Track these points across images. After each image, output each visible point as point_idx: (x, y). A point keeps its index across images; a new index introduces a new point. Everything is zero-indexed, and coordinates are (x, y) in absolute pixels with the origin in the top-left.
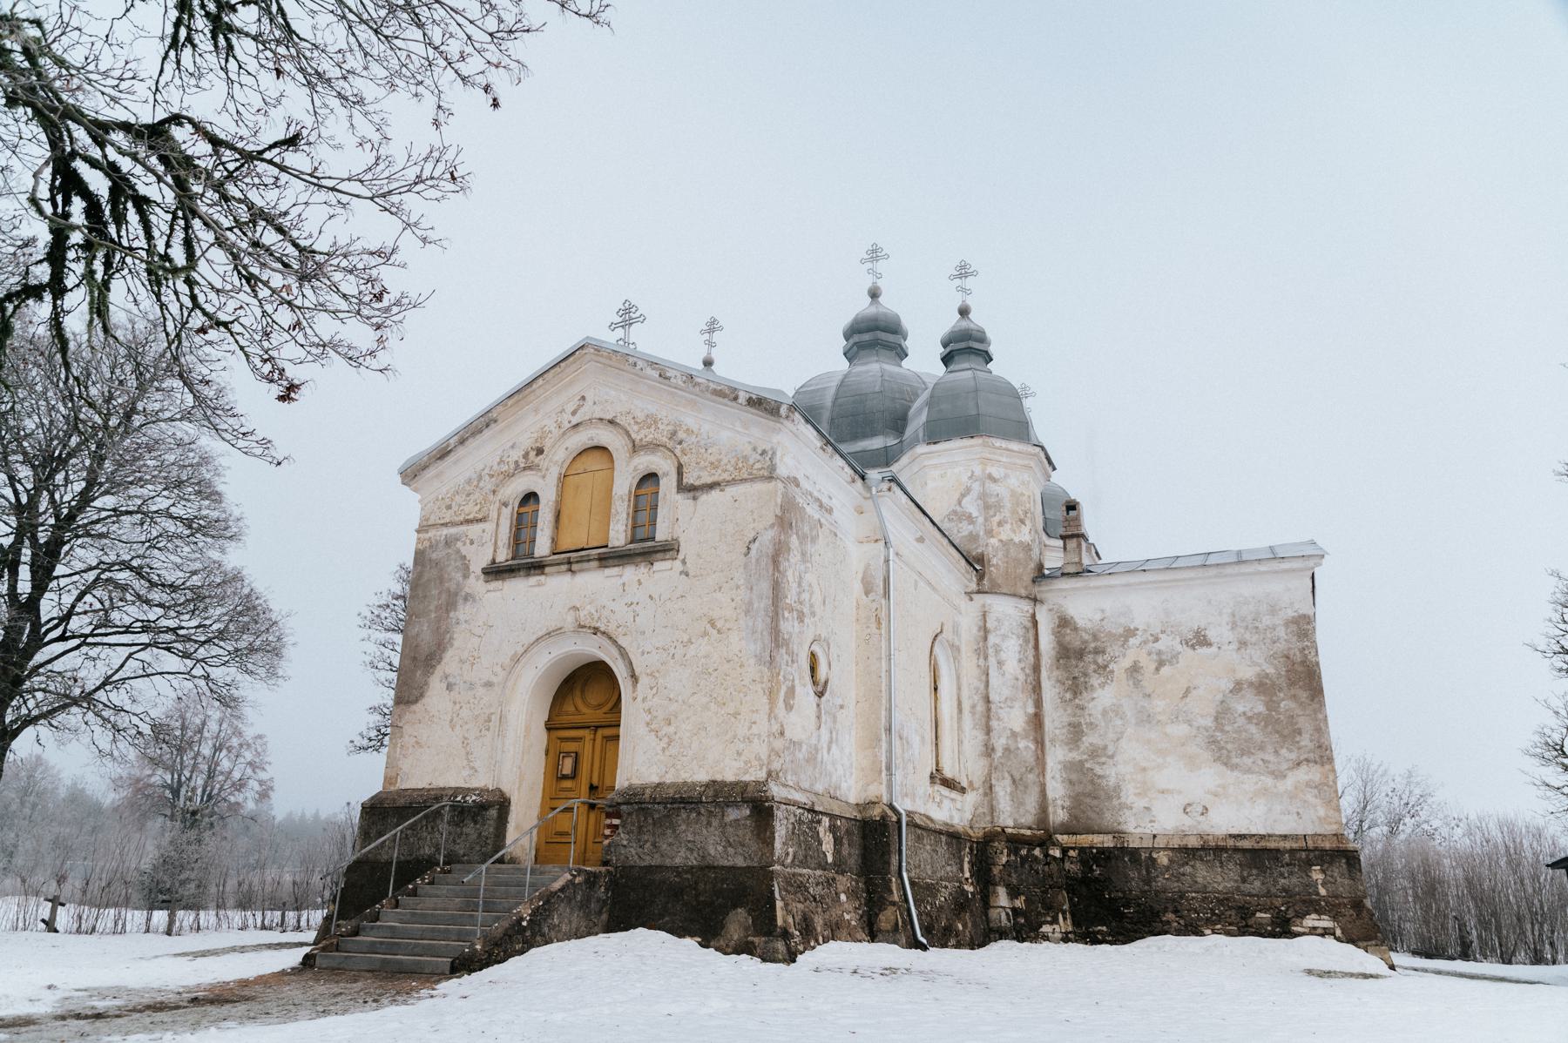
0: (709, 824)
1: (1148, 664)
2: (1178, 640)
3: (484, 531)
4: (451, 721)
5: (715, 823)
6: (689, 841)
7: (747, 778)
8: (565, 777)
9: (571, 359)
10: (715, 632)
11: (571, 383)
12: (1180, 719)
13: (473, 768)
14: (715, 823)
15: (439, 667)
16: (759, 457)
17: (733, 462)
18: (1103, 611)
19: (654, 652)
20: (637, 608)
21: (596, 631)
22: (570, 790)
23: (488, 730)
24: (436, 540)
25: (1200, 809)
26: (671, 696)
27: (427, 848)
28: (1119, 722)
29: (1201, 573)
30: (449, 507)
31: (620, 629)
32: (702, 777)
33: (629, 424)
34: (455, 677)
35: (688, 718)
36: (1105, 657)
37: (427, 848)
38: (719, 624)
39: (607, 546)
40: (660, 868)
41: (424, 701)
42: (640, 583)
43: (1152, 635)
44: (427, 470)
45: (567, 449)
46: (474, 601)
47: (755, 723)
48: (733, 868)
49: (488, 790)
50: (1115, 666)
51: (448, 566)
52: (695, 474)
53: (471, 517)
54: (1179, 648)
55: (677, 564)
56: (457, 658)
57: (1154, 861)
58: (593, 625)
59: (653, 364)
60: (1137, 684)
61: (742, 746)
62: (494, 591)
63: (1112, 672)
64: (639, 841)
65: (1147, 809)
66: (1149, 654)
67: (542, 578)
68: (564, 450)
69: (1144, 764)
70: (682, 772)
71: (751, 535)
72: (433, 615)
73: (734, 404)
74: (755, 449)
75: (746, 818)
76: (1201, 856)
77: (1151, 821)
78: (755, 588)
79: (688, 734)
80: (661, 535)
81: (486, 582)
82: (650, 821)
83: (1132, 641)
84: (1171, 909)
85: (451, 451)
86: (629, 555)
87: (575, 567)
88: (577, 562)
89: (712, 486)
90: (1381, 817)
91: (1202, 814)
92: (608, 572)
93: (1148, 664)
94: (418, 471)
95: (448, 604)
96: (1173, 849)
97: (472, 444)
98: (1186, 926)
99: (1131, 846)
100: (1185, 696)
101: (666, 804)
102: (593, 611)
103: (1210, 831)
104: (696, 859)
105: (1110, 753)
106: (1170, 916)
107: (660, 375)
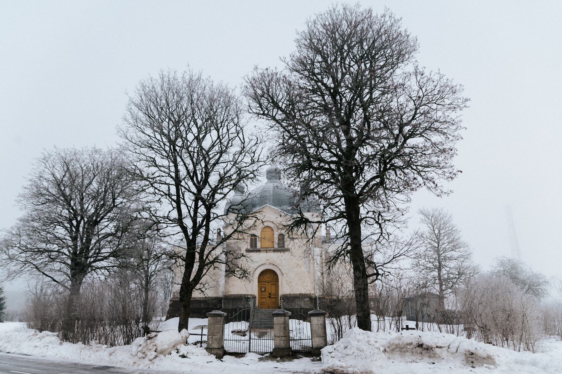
8: (263, 292)
21: (273, 265)
32: (298, 293)
80: (286, 247)
90: (448, 216)
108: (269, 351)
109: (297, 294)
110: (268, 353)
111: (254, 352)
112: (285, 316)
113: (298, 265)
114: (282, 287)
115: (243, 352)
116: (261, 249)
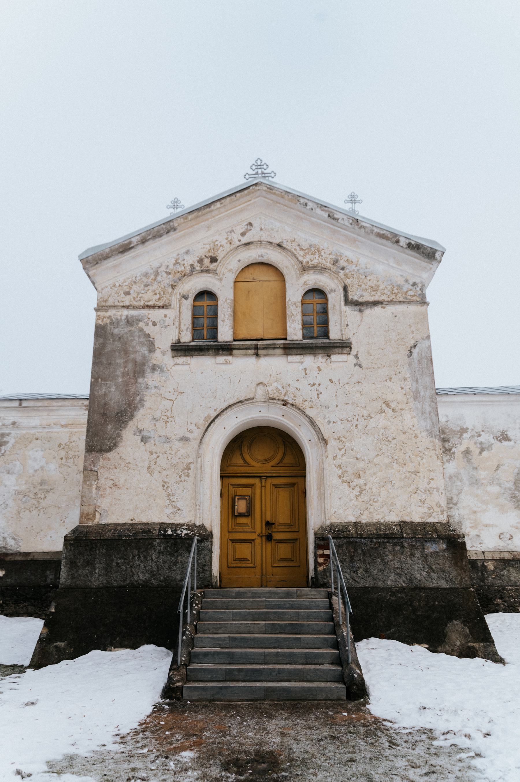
0: (412, 555)
1: (475, 450)
2: (492, 436)
3: (165, 316)
4: (149, 468)
5: (418, 554)
6: (397, 568)
7: (431, 520)
8: (241, 515)
9: (246, 192)
10: (390, 411)
11: (242, 210)
12: (495, 483)
13: (175, 507)
14: (418, 554)
15: (131, 423)
16: (411, 287)
17: (389, 288)
18: (447, 416)
19: (339, 422)
20: (320, 389)
22: (246, 525)
23: (188, 476)
24: (117, 319)
25: (508, 536)
26: (358, 456)
27: (141, 575)
28: (459, 483)
29: (506, 398)
30: (128, 293)
31: (306, 403)
32: (393, 518)
33: (295, 249)
34: (149, 432)
35: (375, 474)
36: (450, 444)
37: (141, 575)
38: (393, 405)
39: (285, 339)
40: (375, 589)
41: (119, 449)
42: (319, 369)
43: (477, 433)
44: (108, 261)
45: (239, 261)
46: (162, 371)
47: (432, 479)
48: (438, 589)
49: (195, 525)
50: (455, 449)
51: (132, 341)
52: (359, 293)
53: (151, 303)
54: (493, 441)
55: (351, 358)
56: (150, 417)
57: (485, 567)
58: (282, 397)
59: (323, 207)
60: (469, 461)
61: (424, 496)
62: (182, 365)
63: (454, 453)
64: (352, 567)
65: (478, 536)
66: (475, 443)
67: (230, 358)
68: (236, 261)
69: (475, 509)
70: (375, 514)
71: (412, 343)
72: (120, 380)
73: (395, 246)
74: (407, 281)
75: (444, 551)
76: (512, 564)
77: (480, 543)
78: (420, 381)
79: (377, 486)
80: (334, 334)
81: (173, 357)
82: (360, 552)
83: (465, 435)
84: (498, 596)
85: (133, 247)
86: (311, 348)
87: (261, 352)
88: (264, 349)
89: (375, 303)
91: (510, 539)
92: (290, 358)
93: (475, 450)
94: (100, 260)
95: (135, 372)
96: (496, 560)
97: (151, 245)
98: (508, 606)
99: (472, 558)
100: (497, 470)
101: (372, 538)
102: (280, 387)
103: (514, 549)
104: (404, 582)
105: (455, 502)
106: (499, 601)
107: (329, 216)
109: (388, 525)
113: (387, 404)
114: (322, 496)
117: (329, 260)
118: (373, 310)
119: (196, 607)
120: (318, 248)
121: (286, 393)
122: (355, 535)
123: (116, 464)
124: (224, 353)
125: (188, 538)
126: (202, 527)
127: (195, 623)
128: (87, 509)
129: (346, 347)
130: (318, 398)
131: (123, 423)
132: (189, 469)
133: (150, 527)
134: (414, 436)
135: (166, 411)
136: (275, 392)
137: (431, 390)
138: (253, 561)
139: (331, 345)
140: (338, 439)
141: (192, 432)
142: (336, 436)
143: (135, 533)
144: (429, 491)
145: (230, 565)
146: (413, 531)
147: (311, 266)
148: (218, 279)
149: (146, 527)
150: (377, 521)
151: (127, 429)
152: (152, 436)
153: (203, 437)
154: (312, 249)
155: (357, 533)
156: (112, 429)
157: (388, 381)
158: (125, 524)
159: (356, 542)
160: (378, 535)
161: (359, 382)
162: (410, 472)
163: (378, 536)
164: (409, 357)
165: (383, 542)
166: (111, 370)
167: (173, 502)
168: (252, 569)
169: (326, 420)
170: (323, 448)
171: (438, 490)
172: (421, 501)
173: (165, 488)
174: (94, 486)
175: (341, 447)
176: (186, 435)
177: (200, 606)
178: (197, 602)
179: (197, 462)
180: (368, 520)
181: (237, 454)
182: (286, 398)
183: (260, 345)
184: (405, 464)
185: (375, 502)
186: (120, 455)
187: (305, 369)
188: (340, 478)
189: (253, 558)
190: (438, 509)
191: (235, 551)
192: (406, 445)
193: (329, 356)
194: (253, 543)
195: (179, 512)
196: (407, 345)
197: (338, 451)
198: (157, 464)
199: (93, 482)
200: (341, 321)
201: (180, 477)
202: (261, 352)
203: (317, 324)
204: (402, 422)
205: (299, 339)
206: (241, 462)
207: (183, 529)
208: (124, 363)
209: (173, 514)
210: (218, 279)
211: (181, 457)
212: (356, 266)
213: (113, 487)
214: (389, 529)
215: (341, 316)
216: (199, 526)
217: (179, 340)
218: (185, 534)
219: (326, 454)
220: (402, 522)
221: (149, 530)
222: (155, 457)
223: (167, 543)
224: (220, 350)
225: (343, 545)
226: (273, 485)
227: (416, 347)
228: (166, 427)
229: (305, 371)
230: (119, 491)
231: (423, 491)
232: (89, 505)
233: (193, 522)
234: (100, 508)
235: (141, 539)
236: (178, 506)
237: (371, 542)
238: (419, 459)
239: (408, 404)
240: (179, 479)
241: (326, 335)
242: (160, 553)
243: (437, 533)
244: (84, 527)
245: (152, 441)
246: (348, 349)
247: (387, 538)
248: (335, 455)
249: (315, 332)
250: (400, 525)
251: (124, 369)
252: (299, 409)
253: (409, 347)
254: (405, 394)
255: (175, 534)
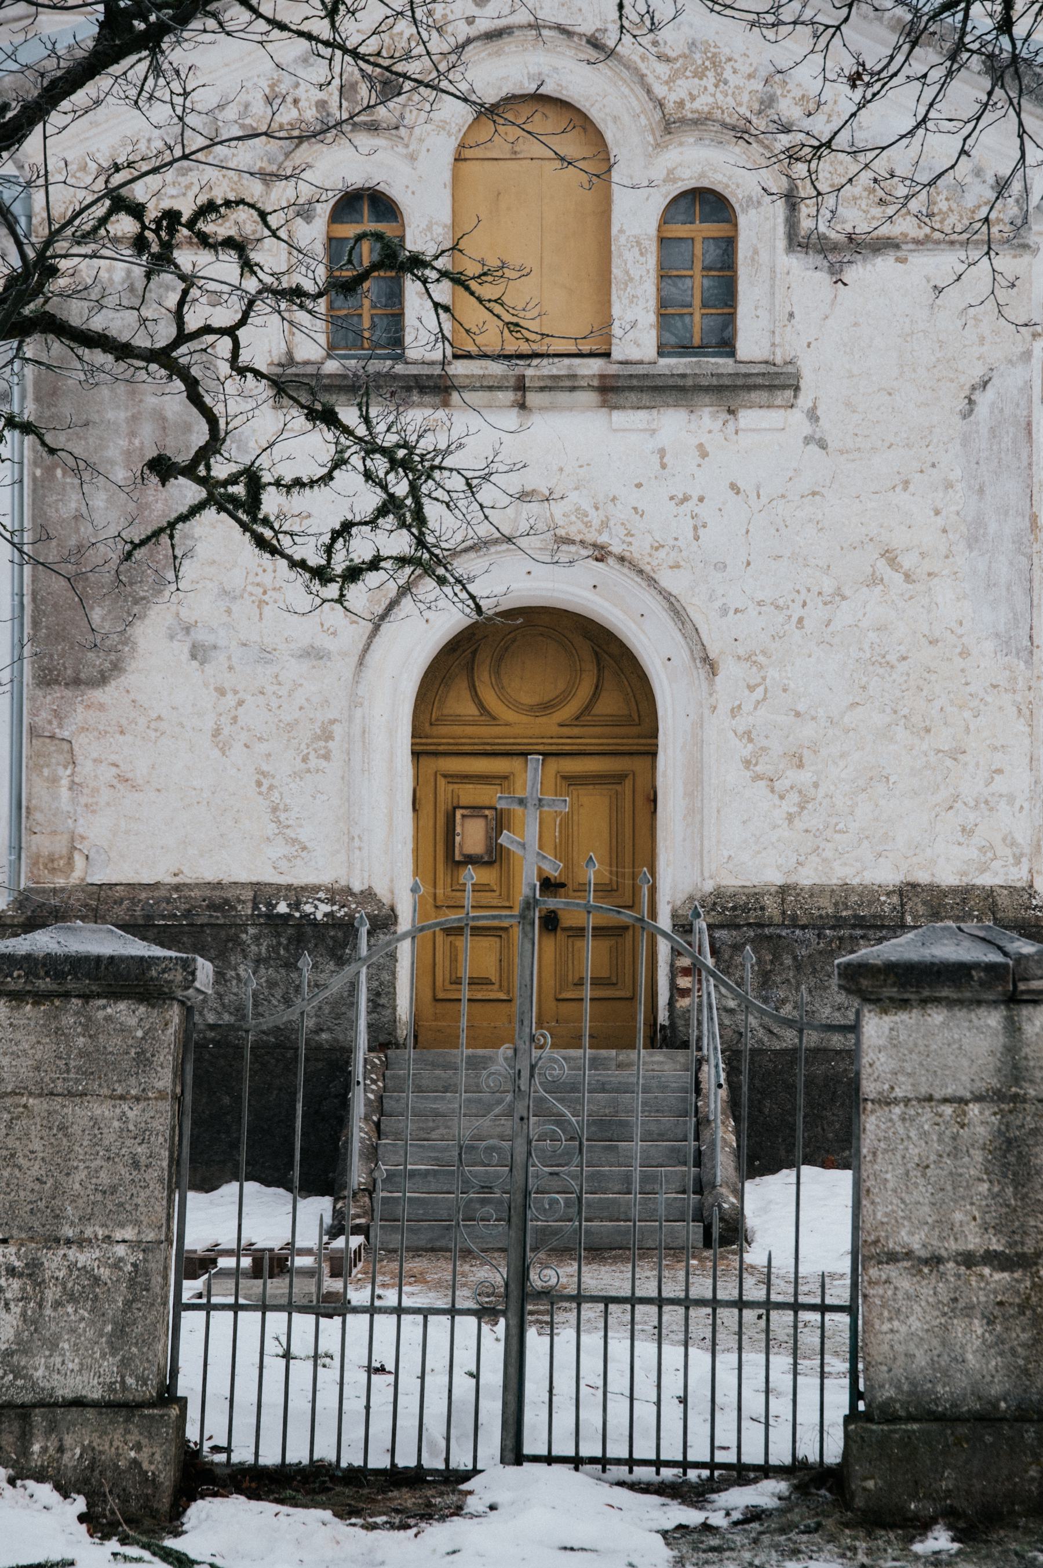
4: (217, 732)
7: (986, 880)
8: (471, 860)
10: (899, 578)
13: (294, 841)
20: (704, 511)
21: (601, 553)
23: (327, 757)
26: (801, 708)
31: (662, 554)
38: (907, 562)
41: (126, 680)
42: (703, 452)
47: (999, 771)
49: (348, 891)
55: (797, 418)
58: (591, 537)
61: (972, 817)
70: (836, 865)
71: (977, 372)
82: (788, 961)
87: (532, 398)
88: (542, 389)
92: (619, 418)
102: (586, 505)
108: (780, 1455)
109: (870, 894)
110: (766, 1471)
111: (576, 1462)
112: (1013, 1000)
113: (890, 557)
114: (694, 812)
115: (433, 1462)
116: (459, 368)
117: (745, 98)
118: (869, 267)
119: (374, 1087)
120: (715, 55)
121: (605, 524)
122: (777, 919)
123: (124, 722)
124: (427, 399)
125: (334, 925)
126: (368, 895)
127: (375, 1118)
128: (47, 844)
129: (784, 387)
130: (697, 538)
131: (136, 602)
132: (329, 737)
133: (229, 895)
134: (958, 650)
135: (260, 571)
136: (573, 518)
137: (1019, 519)
138: (504, 983)
139: (740, 382)
140: (747, 660)
141: (334, 633)
142: (741, 652)
143: (189, 911)
144: (986, 802)
145: (441, 995)
146: (932, 907)
147: (690, 116)
148: (406, 156)
149: (217, 893)
150: (840, 882)
151: (147, 621)
152: (221, 643)
153: (366, 649)
154: (698, 57)
155: (784, 913)
156: (103, 619)
157: (898, 489)
158: (156, 885)
159: (780, 936)
160: (838, 918)
161: (814, 494)
162: (939, 751)
163: (839, 923)
164: (964, 417)
165: (851, 937)
166: (91, 441)
167: (288, 827)
168: (504, 1005)
169: (718, 604)
170: (705, 685)
171: (1011, 799)
172: (964, 830)
173: (264, 789)
174: (65, 782)
175: (752, 682)
176: (317, 644)
177: (380, 1084)
178: (374, 1076)
179: (351, 719)
180: (818, 881)
181: (461, 686)
182: (602, 539)
183: (532, 377)
184: (928, 730)
185: (840, 832)
186: (132, 696)
187: (662, 452)
188: (747, 768)
189: (505, 976)
190: (1008, 852)
191: (454, 959)
192: (933, 677)
193: (731, 412)
194: (504, 935)
195: (304, 854)
196: (963, 379)
197: (747, 692)
198: (240, 723)
199: (61, 771)
200: (773, 304)
201: (305, 759)
202: (532, 398)
203: (704, 306)
204: (929, 612)
205: (646, 359)
206: (470, 709)
207: (319, 899)
208: (127, 421)
209: (289, 860)
210: (406, 156)
211: (306, 705)
212: (828, 121)
213: (118, 786)
214: (870, 903)
215: (772, 286)
216: (362, 892)
217: (290, 354)
218: (326, 915)
219: (713, 701)
220: (908, 884)
221: (227, 901)
222: (233, 703)
223: (278, 935)
224: (415, 392)
225: (744, 944)
226: (564, 778)
227: (989, 386)
228: (261, 618)
229: (662, 458)
230: (136, 795)
231: (972, 804)
232: (54, 833)
233: (343, 883)
234: (86, 843)
235: (207, 925)
236: (303, 838)
237: (819, 936)
238: (967, 714)
239: (951, 559)
240: (303, 766)
241: (726, 346)
242: (258, 961)
243: (993, 913)
244: (44, 891)
245: (222, 657)
246: (789, 393)
247: (862, 927)
248: (737, 703)
249: (697, 330)
250: (901, 895)
251: (130, 442)
252: (641, 572)
253: (968, 386)
254: (945, 531)
255: (297, 915)
